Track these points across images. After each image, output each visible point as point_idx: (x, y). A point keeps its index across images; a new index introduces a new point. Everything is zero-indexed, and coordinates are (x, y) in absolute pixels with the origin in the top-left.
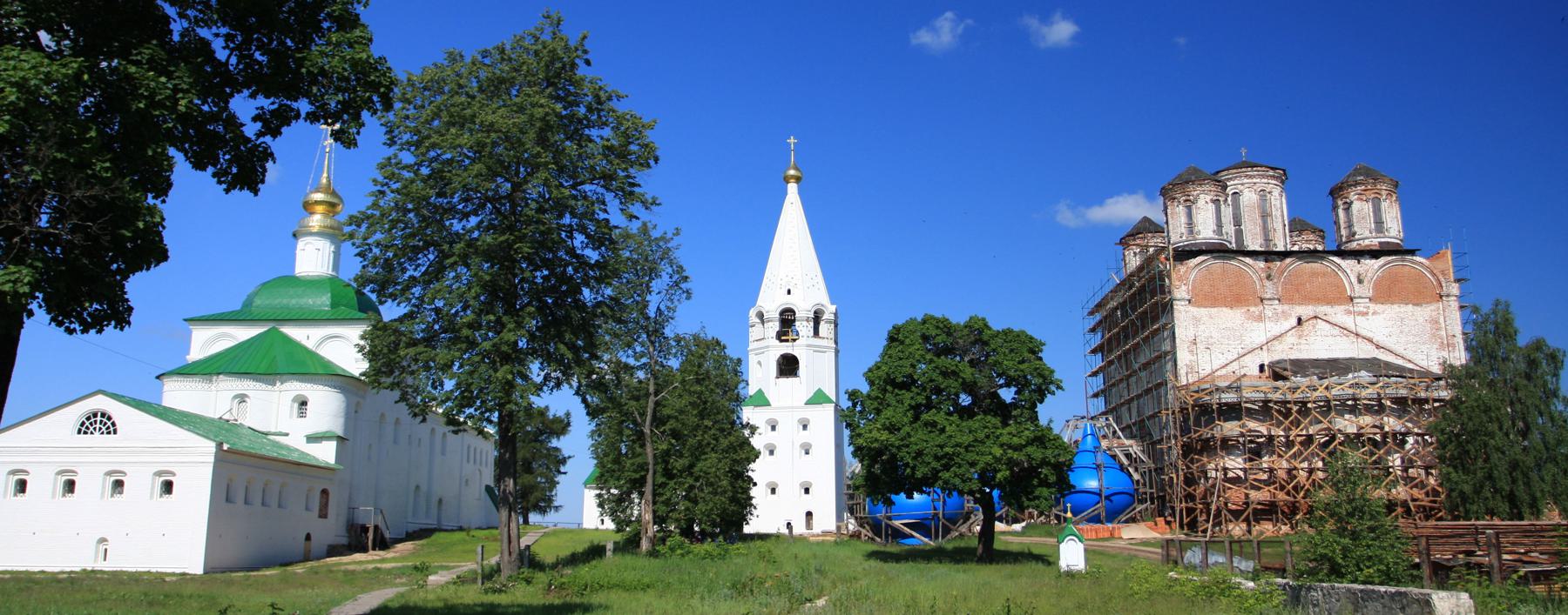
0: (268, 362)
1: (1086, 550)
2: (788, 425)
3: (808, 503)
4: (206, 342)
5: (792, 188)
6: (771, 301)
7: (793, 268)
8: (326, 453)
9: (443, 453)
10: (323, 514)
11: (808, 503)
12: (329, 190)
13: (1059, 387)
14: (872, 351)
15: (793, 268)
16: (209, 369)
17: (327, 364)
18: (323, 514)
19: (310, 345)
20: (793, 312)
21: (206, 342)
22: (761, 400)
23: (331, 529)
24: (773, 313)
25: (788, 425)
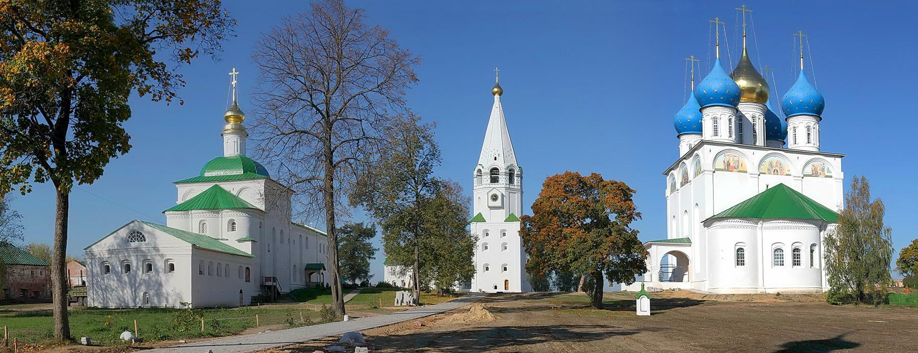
0: (214, 202)
1: (635, 310)
2: (495, 234)
3: (506, 275)
4: (187, 192)
5: (497, 97)
6: (486, 162)
7: (495, 146)
8: (246, 248)
9: (307, 248)
10: (248, 280)
11: (506, 275)
12: (498, 87)
13: (856, 180)
14: (535, 193)
15: (495, 146)
16: (186, 207)
17: (242, 202)
18: (248, 280)
19: (234, 193)
20: (497, 169)
21: (187, 192)
22: (480, 219)
23: (252, 289)
24: (486, 170)
25: (495, 234)
